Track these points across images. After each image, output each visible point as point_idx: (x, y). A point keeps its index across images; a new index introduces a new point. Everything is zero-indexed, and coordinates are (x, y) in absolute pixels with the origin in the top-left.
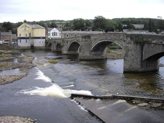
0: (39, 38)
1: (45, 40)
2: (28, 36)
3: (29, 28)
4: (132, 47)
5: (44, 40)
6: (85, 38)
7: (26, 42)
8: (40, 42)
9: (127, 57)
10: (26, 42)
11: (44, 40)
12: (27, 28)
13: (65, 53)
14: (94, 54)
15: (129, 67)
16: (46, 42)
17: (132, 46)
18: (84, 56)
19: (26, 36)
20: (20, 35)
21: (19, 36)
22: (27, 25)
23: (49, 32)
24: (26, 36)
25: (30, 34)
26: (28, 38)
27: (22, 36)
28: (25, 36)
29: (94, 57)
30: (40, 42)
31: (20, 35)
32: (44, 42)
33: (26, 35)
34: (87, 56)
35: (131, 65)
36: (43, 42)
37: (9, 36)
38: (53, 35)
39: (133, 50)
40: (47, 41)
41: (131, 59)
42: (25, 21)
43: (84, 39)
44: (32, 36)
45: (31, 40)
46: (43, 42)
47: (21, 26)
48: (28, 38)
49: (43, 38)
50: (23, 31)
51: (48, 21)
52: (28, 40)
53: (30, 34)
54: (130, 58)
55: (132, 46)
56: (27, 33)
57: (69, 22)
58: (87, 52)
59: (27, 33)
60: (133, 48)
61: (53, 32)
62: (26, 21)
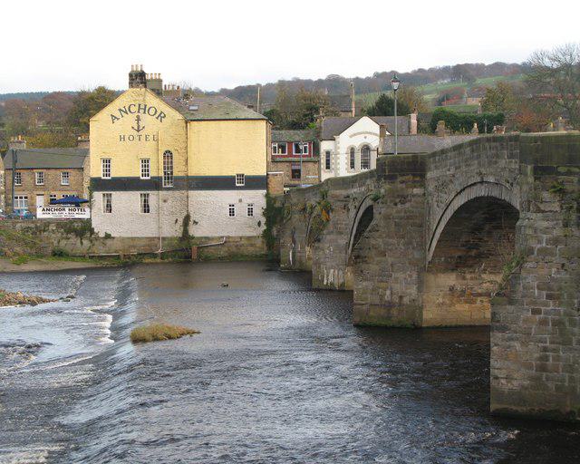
0: (224, 183)
1: (267, 196)
2: (156, 170)
3: (161, 116)
4: (547, 230)
5: (257, 198)
6: (391, 178)
7: (146, 209)
8: (232, 213)
9: (511, 302)
10: (146, 209)
11: (257, 198)
12: (148, 120)
13: (331, 279)
14: (452, 289)
15: (532, 378)
16: (274, 213)
17: (545, 224)
18: (382, 297)
19: (146, 170)
20: (107, 162)
21: (95, 170)
22: (152, 101)
23: (325, 146)
24: (146, 170)
25: (168, 155)
26: (155, 184)
27: (117, 172)
28: (136, 172)
29: (458, 307)
30: (232, 213)
31: (107, 162)
32: (258, 212)
33: (145, 162)
34: (406, 300)
35: (543, 368)
36: (250, 212)
37: (72, 173)
38: (352, 165)
39: (552, 254)
40: (278, 204)
41: (543, 322)
42: (138, 78)
43: (387, 186)
44: (178, 171)
45: (177, 193)
46: (250, 212)
47: (112, 109)
48: (155, 184)
49: (253, 183)
50: (122, 138)
51: (431, 70)
52: (154, 197)
53: (168, 155)
54: (535, 312)
55: (545, 224)
56: (148, 150)
57: (519, 80)
58: (400, 275)
59: (148, 150)
60: (556, 241)
61: (358, 142)
62: (142, 75)
